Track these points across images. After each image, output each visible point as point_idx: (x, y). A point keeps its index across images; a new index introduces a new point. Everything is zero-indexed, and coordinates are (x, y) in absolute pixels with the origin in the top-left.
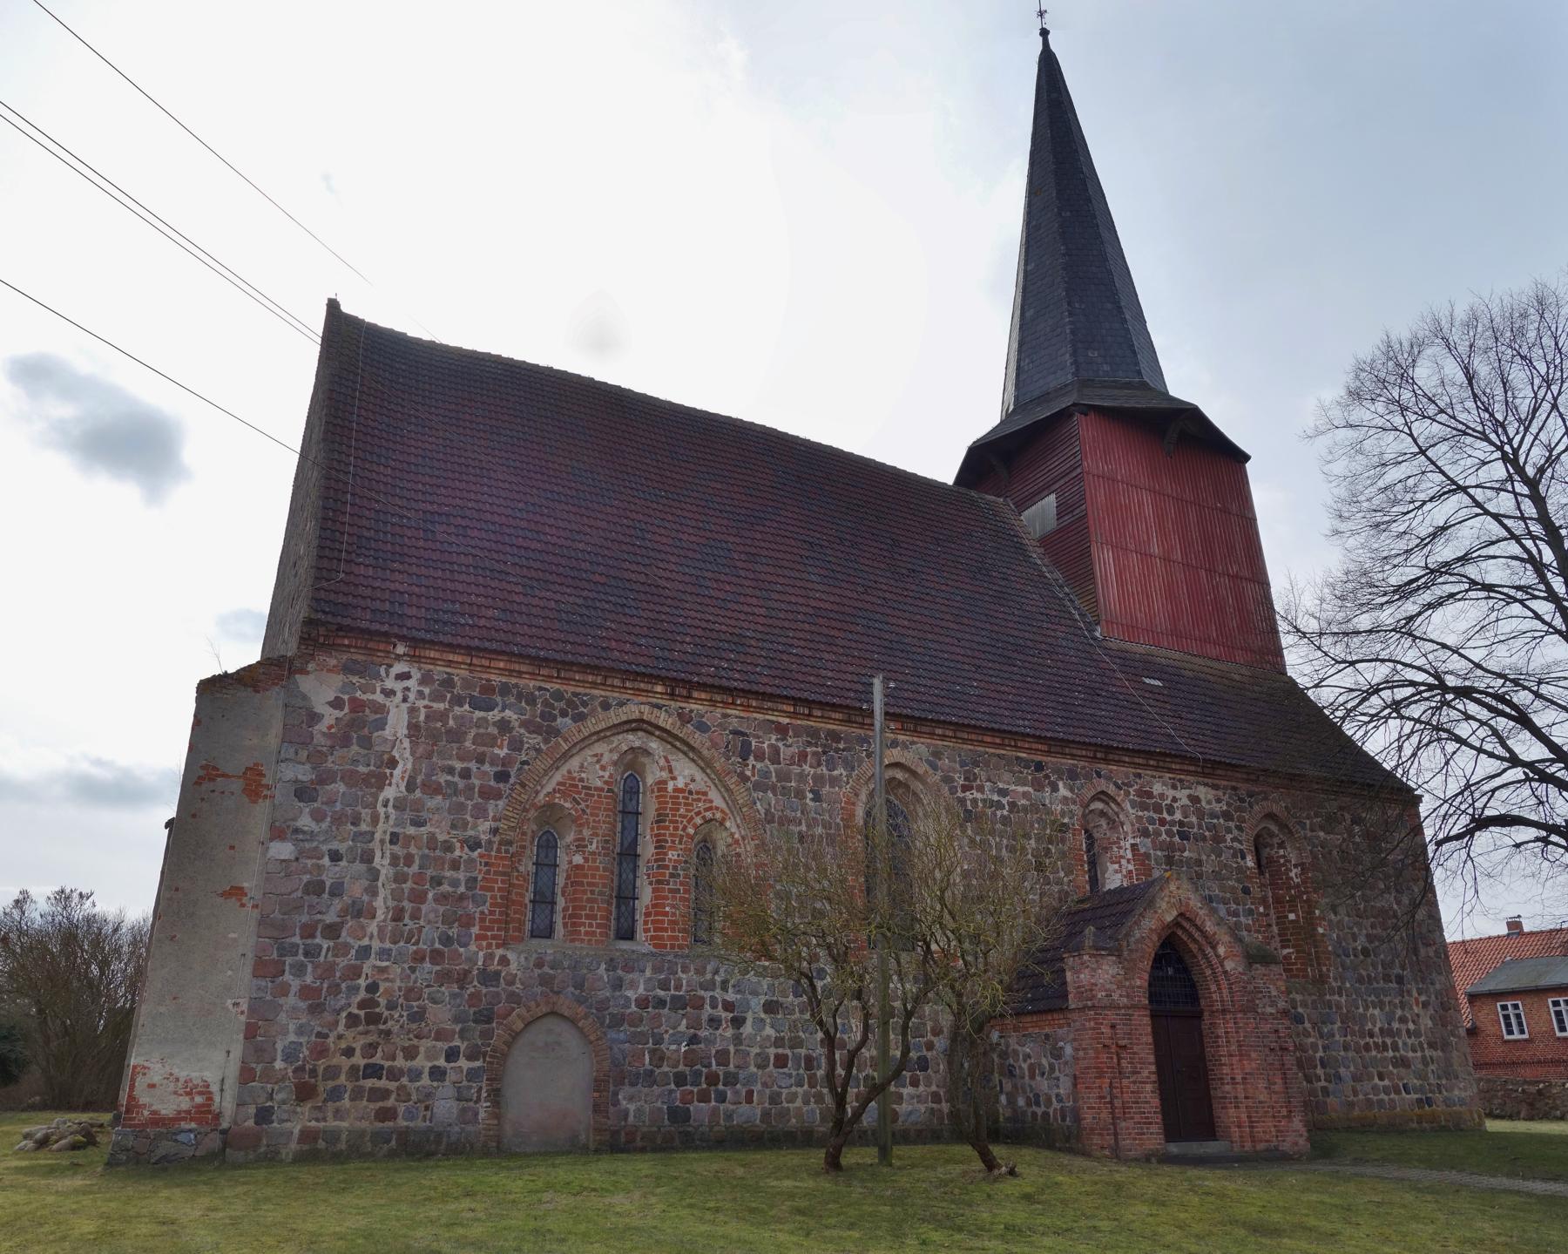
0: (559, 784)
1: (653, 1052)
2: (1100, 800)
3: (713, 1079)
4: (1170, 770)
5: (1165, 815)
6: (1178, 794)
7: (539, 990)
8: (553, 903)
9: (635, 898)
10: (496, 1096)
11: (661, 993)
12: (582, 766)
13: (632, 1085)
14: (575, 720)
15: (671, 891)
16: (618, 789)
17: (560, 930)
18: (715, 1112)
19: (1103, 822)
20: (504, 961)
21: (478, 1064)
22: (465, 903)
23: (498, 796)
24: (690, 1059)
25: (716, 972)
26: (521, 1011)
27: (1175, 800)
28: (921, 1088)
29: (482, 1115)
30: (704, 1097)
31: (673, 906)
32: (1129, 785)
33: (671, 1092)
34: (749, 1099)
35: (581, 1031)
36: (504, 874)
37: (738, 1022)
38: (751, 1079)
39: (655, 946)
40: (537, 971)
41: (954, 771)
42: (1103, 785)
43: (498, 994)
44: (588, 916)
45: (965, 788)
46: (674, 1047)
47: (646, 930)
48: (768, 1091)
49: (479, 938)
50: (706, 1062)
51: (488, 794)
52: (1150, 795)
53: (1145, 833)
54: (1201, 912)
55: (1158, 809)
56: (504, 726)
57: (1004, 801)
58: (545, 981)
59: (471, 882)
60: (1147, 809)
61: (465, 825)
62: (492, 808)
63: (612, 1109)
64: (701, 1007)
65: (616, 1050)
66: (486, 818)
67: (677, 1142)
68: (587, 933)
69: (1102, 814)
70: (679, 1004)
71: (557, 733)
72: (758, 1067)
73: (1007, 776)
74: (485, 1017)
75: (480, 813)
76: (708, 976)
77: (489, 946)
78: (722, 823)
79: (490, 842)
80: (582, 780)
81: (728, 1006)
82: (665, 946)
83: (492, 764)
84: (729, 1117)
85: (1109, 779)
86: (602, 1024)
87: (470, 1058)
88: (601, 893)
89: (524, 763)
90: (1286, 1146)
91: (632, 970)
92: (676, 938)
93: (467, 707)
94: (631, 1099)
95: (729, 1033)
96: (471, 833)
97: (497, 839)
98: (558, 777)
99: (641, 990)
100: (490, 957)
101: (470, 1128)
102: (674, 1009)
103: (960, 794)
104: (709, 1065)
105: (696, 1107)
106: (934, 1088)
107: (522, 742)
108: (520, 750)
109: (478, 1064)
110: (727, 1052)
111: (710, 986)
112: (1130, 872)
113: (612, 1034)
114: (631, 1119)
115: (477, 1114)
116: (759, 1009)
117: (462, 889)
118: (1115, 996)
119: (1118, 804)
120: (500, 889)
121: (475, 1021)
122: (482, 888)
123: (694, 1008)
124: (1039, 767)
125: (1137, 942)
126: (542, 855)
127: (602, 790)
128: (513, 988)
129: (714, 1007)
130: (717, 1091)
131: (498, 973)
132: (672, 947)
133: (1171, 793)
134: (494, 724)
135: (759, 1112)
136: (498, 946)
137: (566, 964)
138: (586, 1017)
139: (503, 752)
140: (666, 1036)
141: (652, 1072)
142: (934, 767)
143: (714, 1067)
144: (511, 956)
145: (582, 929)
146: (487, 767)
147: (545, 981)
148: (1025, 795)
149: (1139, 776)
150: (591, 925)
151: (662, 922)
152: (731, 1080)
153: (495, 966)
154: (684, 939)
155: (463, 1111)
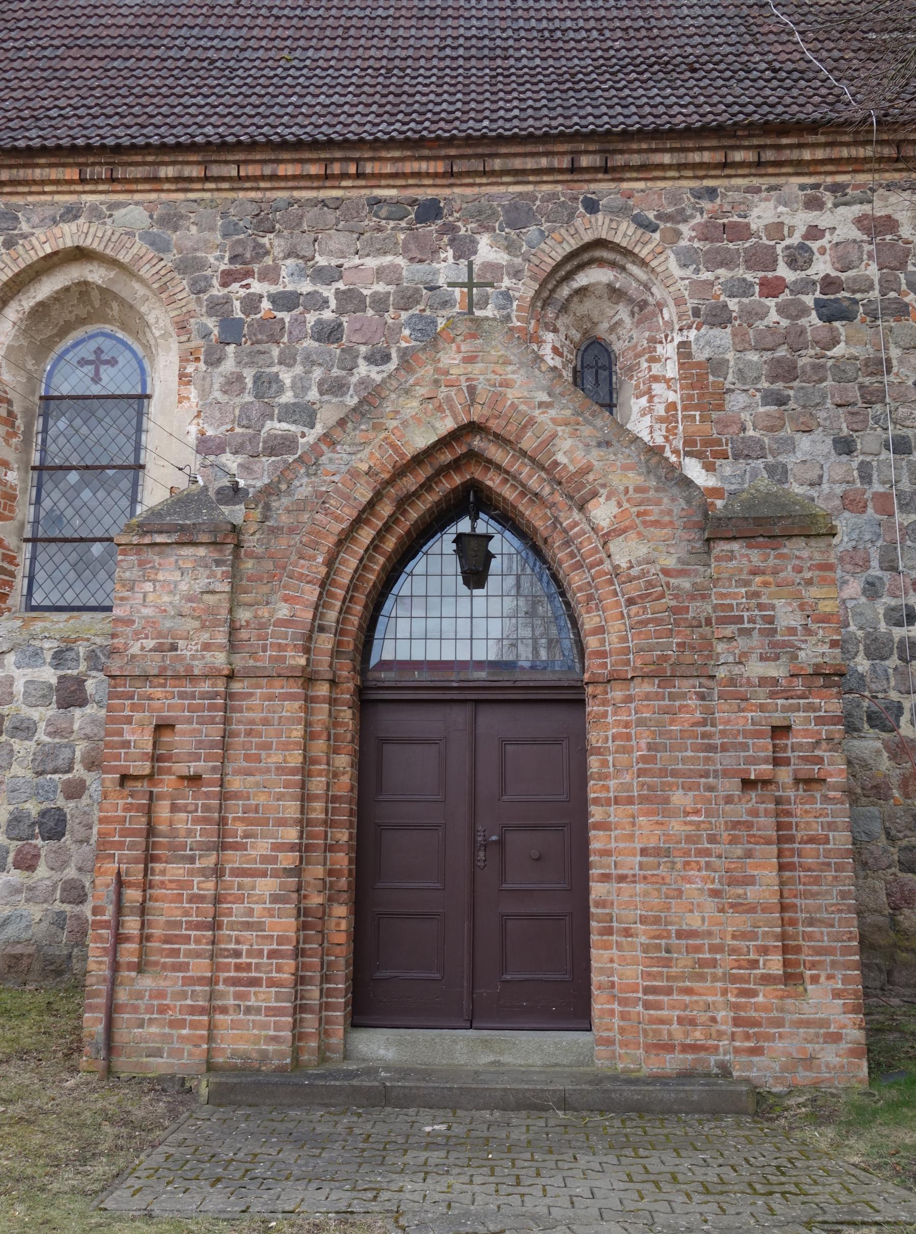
2: (601, 262)
4: (800, 167)
5: (783, 271)
6: (823, 219)
19: (623, 312)
27: (814, 233)
28: (42, 870)
32: (681, 217)
41: (208, 246)
42: (598, 226)
45: (228, 278)
52: (740, 232)
53: (718, 317)
54: (544, 417)
55: (762, 259)
57: (328, 292)
60: (727, 262)
69: (615, 293)
73: (338, 240)
85: (622, 211)
90: (764, 1070)
103: (217, 291)
106: (71, 873)
112: (671, 406)
118: (187, 650)
119: (643, 263)
124: (430, 211)
125: (302, 506)
133: (802, 219)
142: (160, 246)
148: (380, 274)
149: (712, 193)
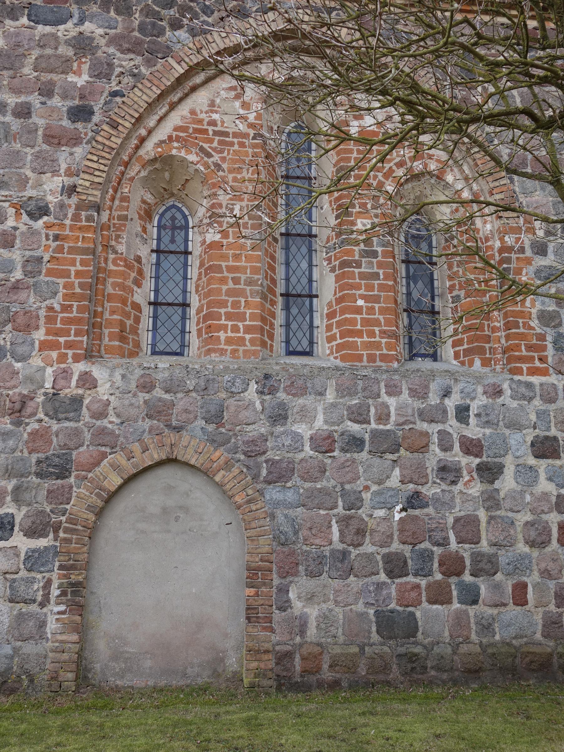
0: (176, 129)
1: (344, 521)
3: (452, 566)
7: (147, 424)
8: (185, 305)
9: (311, 296)
10: (76, 594)
11: (355, 428)
12: (212, 104)
13: (311, 575)
14: (193, 32)
15: (363, 276)
16: (279, 143)
17: (194, 341)
18: (460, 620)
20: (87, 381)
21: (42, 543)
22: (22, 295)
23: (75, 140)
24: (411, 533)
25: (447, 393)
26: (120, 458)
29: (52, 626)
30: (439, 596)
31: (365, 298)
33: (380, 586)
34: (520, 595)
35: (220, 486)
36: (84, 251)
37: (490, 472)
38: (519, 566)
39: (343, 358)
40: (143, 396)
43: (77, 432)
44: (229, 317)
46: (381, 513)
47: (330, 339)
48: (552, 584)
49: (45, 346)
50: (438, 536)
51: (55, 139)
56: (83, 45)
58: (156, 411)
59: (33, 264)
61: (23, 182)
62: (63, 159)
63: (277, 615)
64: (424, 448)
65: (281, 518)
66: (55, 173)
67: (395, 672)
68: (229, 341)
70: (387, 444)
71: (167, 52)
72: (532, 544)
74: (58, 468)
75: (46, 166)
76: (434, 399)
77: (62, 358)
78: (440, 178)
79: (62, 206)
80: (213, 123)
81: (471, 447)
82: (359, 358)
83: (64, 97)
84: (486, 627)
86: (255, 477)
87: (31, 533)
88: (249, 282)
89: (114, 94)
91: (303, 392)
92: (377, 345)
93: (24, 20)
94: (310, 598)
95: (476, 489)
96: (30, 192)
97: (74, 200)
98: (176, 119)
99: (319, 422)
100: (66, 374)
101: (29, 648)
102: (377, 453)
104: (444, 543)
105: (425, 612)
107: (110, 65)
108: (108, 77)
109: (42, 543)
110: (473, 521)
111: (435, 415)
113: (273, 493)
114: (312, 632)
115: (42, 624)
116: (525, 451)
117: (18, 274)
120: (78, 274)
121: (39, 475)
122: (50, 273)
123: (412, 450)
126: (166, 239)
127: (245, 136)
128: (105, 422)
129: (446, 447)
130: (462, 587)
131: (77, 401)
132: (372, 358)
134: (68, 43)
135: (539, 618)
136: (77, 359)
137: (190, 384)
138: (228, 466)
139: (82, 80)
140: (367, 496)
141: (345, 554)
143: (453, 545)
144: (98, 372)
145: (222, 335)
146: (56, 101)
147: (156, 411)
150: (235, 329)
151: (353, 322)
152: (485, 566)
153: (72, 389)
154: (389, 347)
155: (21, 618)
